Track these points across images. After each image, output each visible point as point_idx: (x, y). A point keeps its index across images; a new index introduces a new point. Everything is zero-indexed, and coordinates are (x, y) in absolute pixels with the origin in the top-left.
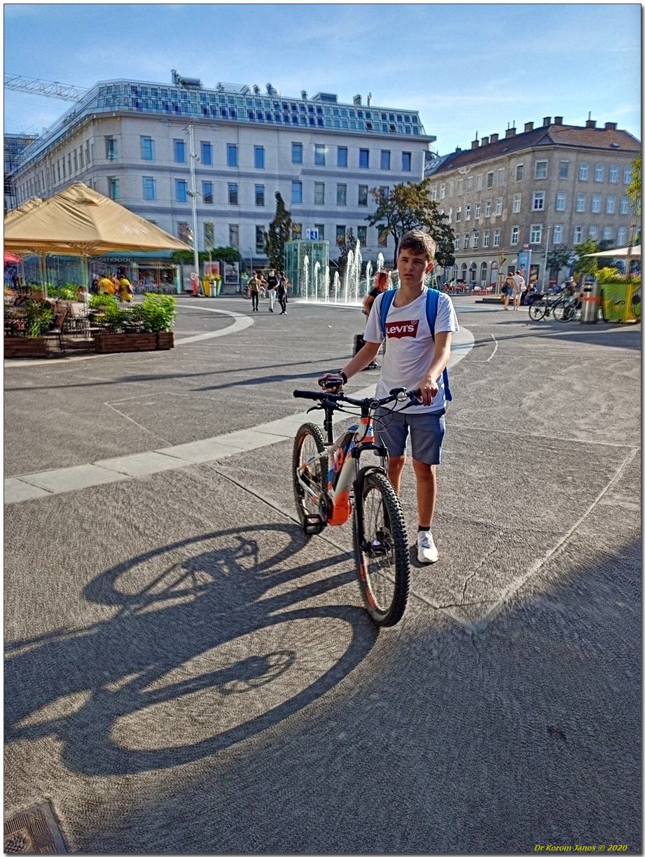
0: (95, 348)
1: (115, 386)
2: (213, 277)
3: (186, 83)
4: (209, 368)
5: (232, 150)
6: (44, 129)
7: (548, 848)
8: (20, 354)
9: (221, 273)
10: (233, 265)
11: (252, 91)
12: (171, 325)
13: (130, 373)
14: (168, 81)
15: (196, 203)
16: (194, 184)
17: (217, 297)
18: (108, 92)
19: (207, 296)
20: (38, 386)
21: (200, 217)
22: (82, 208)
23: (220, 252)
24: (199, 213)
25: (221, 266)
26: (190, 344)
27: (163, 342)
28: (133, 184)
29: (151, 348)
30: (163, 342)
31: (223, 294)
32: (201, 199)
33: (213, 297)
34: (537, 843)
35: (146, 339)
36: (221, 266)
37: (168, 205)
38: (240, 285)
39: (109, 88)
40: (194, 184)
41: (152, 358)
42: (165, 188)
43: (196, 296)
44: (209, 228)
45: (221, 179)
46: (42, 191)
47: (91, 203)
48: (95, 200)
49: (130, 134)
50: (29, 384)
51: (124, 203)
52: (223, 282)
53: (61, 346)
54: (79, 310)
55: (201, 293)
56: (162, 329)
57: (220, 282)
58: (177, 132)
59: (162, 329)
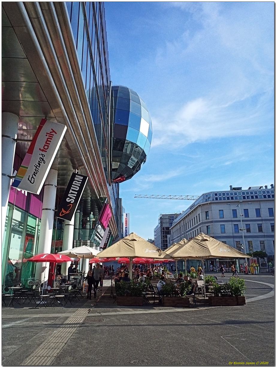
0: (208, 303)
1: (224, 326)
2: (255, 265)
3: (234, 189)
4: (268, 318)
5: (258, 211)
6: (183, 211)
7: (235, 363)
8: (178, 305)
9: (258, 263)
10: (264, 259)
11: (264, 188)
12: (244, 294)
13: (229, 319)
14: (229, 189)
15: (244, 233)
16: (242, 226)
17: (258, 274)
18: (206, 196)
19: (253, 274)
20: (189, 323)
21: (245, 239)
22: (203, 243)
23: (257, 253)
24: (245, 237)
25: (258, 259)
26: (252, 302)
27: (241, 302)
28: (217, 228)
29: (234, 304)
30: (241, 302)
31: (261, 273)
32: (246, 231)
33: (256, 274)
34: (230, 361)
35: (232, 300)
36: (258, 259)
37: (231, 235)
38: (268, 268)
39: (207, 196)
40: (242, 226)
41: (237, 310)
42: (229, 228)
43: (247, 274)
44: (250, 243)
45: (254, 222)
46: (182, 233)
47: (206, 240)
48: (208, 239)
49: (215, 210)
50: (186, 322)
51: (212, 236)
52: (260, 267)
53: (194, 301)
54: (200, 283)
55: (250, 273)
56: (239, 295)
57: (259, 267)
58: (234, 207)
59: (239, 295)
